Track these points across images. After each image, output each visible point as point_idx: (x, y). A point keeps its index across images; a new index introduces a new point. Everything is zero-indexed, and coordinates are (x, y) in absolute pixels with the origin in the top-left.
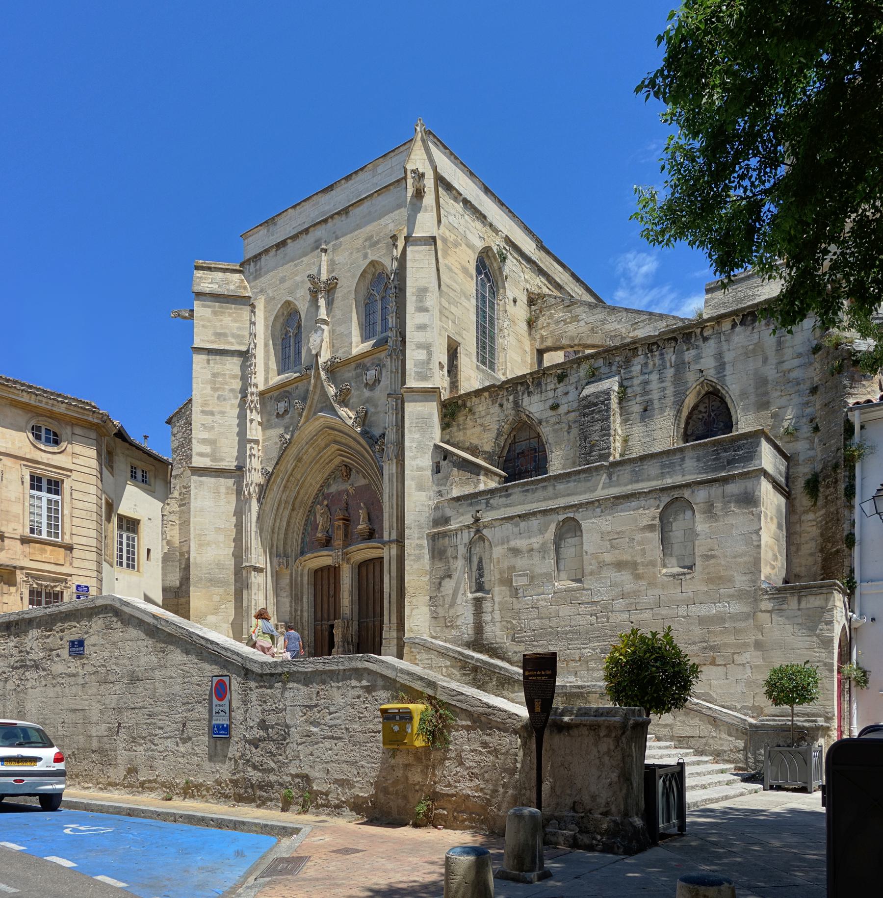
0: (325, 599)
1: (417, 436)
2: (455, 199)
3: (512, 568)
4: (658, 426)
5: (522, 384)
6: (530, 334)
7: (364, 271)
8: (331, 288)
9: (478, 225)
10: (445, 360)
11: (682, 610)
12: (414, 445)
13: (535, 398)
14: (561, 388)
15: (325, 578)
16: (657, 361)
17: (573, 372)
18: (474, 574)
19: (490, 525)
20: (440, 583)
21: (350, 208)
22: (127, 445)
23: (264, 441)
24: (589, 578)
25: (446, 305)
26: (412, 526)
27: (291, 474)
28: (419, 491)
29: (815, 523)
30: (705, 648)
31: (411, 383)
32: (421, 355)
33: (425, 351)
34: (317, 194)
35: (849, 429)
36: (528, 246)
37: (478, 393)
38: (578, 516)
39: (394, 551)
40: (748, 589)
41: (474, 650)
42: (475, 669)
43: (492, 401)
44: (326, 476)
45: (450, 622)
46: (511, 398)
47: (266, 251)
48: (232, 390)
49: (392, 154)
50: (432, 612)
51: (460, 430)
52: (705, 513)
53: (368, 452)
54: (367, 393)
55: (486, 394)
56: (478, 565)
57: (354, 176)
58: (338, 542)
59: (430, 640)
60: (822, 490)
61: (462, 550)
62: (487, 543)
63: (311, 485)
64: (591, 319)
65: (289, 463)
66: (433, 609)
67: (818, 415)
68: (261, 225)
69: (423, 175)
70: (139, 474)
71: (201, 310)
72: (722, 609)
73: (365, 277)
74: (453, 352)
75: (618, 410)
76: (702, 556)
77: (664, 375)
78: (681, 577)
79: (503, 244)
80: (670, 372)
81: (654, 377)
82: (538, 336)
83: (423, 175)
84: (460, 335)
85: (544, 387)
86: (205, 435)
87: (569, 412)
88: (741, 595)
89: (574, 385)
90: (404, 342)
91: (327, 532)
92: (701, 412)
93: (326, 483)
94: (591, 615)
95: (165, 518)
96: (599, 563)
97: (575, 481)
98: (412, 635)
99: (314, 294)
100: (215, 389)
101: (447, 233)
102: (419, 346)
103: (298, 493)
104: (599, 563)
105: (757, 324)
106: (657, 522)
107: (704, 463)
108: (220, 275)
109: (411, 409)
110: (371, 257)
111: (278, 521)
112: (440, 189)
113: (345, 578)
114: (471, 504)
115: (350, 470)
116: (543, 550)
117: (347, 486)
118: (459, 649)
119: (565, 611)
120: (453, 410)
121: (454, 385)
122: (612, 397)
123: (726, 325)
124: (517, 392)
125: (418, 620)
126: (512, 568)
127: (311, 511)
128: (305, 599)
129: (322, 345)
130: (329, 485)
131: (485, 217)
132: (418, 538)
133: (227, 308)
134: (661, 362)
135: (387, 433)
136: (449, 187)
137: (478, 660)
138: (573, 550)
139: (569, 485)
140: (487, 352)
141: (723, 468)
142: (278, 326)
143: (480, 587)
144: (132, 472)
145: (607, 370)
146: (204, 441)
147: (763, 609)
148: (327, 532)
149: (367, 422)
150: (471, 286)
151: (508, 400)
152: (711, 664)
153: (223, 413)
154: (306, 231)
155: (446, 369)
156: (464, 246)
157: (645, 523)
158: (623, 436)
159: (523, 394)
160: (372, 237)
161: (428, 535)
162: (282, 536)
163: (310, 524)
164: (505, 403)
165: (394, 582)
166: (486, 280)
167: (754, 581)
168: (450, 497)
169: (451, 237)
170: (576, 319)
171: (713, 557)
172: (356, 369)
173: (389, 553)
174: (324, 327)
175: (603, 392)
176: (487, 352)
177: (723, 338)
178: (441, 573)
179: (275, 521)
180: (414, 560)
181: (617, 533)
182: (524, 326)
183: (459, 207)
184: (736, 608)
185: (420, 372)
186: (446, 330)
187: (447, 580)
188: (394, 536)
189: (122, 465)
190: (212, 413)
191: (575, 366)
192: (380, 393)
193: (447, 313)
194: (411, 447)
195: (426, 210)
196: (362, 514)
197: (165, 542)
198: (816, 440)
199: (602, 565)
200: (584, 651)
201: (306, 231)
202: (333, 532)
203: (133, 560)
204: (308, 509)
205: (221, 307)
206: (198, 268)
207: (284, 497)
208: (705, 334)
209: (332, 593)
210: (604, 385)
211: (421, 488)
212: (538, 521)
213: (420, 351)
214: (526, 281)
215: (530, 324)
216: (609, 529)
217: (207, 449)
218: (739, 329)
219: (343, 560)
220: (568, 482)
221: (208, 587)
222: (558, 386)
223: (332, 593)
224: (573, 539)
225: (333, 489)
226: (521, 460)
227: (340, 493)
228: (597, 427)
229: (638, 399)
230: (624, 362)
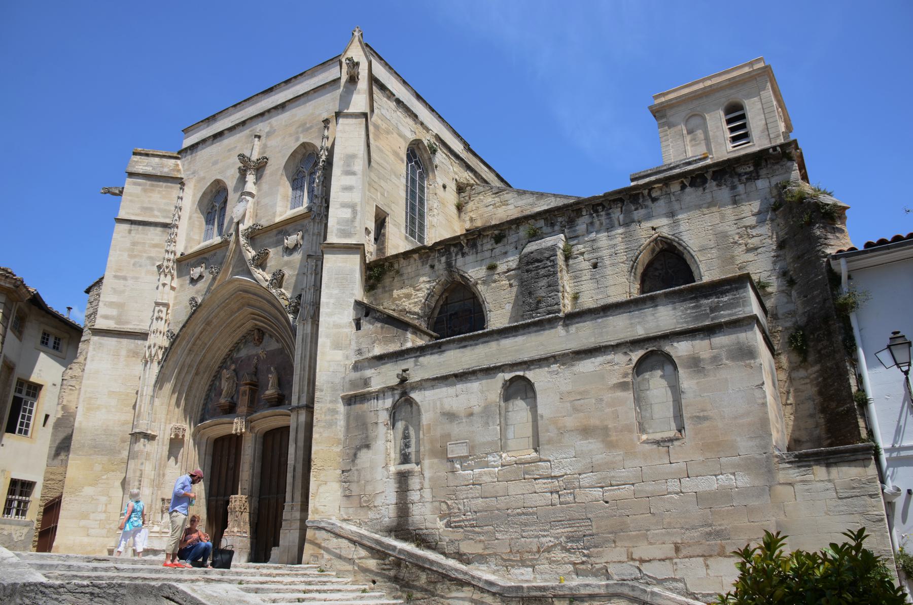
0: (224, 471)
1: (336, 292)
2: (389, 98)
3: (447, 437)
4: (611, 282)
5: (455, 245)
6: (459, 217)
7: (295, 152)
8: (260, 167)
9: (410, 121)
10: (372, 226)
11: (673, 485)
12: (332, 301)
14: (499, 248)
16: (603, 218)
17: (512, 232)
19: (421, 385)
20: (355, 455)
22: (43, 313)
23: (174, 304)
24: (546, 447)
25: (376, 179)
26: (325, 387)
27: (198, 338)
28: (335, 349)
29: (808, 381)
30: (709, 534)
31: (332, 239)
32: (347, 214)
33: (350, 210)
35: (835, 279)
36: (458, 147)
37: (406, 255)
38: (529, 375)
39: (303, 417)
40: (758, 457)
41: (397, 537)
42: (398, 563)
43: (423, 263)
44: (235, 341)
45: (365, 502)
46: (443, 259)
48: (322, 391)
50: (345, 489)
51: (385, 292)
52: (689, 367)
55: (416, 256)
56: (404, 433)
58: (242, 409)
59: (339, 524)
60: (812, 344)
63: (219, 349)
64: (520, 203)
65: (197, 327)
66: (346, 485)
67: (790, 268)
69: (358, 64)
70: (51, 342)
71: (131, 187)
72: (727, 483)
74: (381, 221)
75: (564, 267)
76: (692, 418)
78: (667, 444)
79: (433, 140)
82: (468, 218)
83: (358, 64)
84: (389, 207)
85: (479, 248)
86: (114, 298)
87: (509, 271)
88: (749, 466)
89: (514, 245)
90: (327, 202)
91: (232, 398)
92: (656, 269)
93: (236, 347)
94: (552, 493)
95: (65, 382)
96: (559, 429)
98: (317, 517)
99: (243, 173)
100: (131, 256)
101: (380, 122)
102: (344, 205)
103: (204, 356)
104: (559, 429)
105: (707, 185)
107: (682, 311)
108: (157, 160)
109: (331, 262)
112: (374, 87)
113: (246, 448)
115: (263, 334)
116: (486, 412)
117: (259, 351)
118: (377, 536)
119: (516, 488)
120: (378, 273)
121: (381, 249)
122: (558, 253)
123: (675, 187)
124: (450, 254)
125: (326, 499)
126: (447, 437)
127: (217, 376)
129: (244, 212)
130: (239, 350)
131: (416, 116)
132: (331, 402)
133: (157, 186)
134: (608, 221)
135: (303, 293)
136: (383, 87)
137: (401, 551)
140: (416, 219)
141: (706, 316)
142: (206, 201)
143: (405, 459)
144: (43, 338)
145: (549, 230)
146: (111, 304)
147: (782, 481)
148: (232, 398)
150: (402, 168)
151: (440, 261)
152: (719, 555)
153: (136, 279)
155: (372, 236)
156: (395, 135)
158: (575, 287)
159: (456, 255)
161: (343, 398)
163: (213, 389)
164: (437, 264)
165: (301, 453)
166: (416, 167)
167: (765, 447)
168: (371, 355)
169: (383, 126)
170: (505, 203)
171: (706, 418)
173: (295, 421)
174: (248, 198)
175: (547, 249)
176: (416, 219)
177: (673, 198)
178: (357, 443)
180: (324, 427)
181: (580, 393)
182: (454, 210)
183: (393, 105)
184: (743, 481)
185: (344, 230)
186: (374, 200)
188: (304, 401)
189: (33, 332)
190: (125, 278)
191: (514, 227)
193: (376, 186)
194: (328, 304)
195: (359, 93)
196: (272, 378)
197: (60, 406)
198: (794, 293)
199: (562, 432)
200: (543, 540)
202: (238, 398)
203: (28, 425)
205: (152, 185)
207: (188, 361)
208: (654, 195)
209: (231, 465)
210: (548, 242)
211: (337, 346)
213: (345, 210)
214: (456, 173)
215: (460, 208)
216: (570, 388)
217: (114, 312)
218: (689, 190)
220: (516, 336)
221: (90, 455)
222: (495, 246)
223: (231, 465)
225: (243, 353)
226: (456, 317)
227: (249, 358)
228: (543, 282)
229: (586, 256)
230: (568, 222)
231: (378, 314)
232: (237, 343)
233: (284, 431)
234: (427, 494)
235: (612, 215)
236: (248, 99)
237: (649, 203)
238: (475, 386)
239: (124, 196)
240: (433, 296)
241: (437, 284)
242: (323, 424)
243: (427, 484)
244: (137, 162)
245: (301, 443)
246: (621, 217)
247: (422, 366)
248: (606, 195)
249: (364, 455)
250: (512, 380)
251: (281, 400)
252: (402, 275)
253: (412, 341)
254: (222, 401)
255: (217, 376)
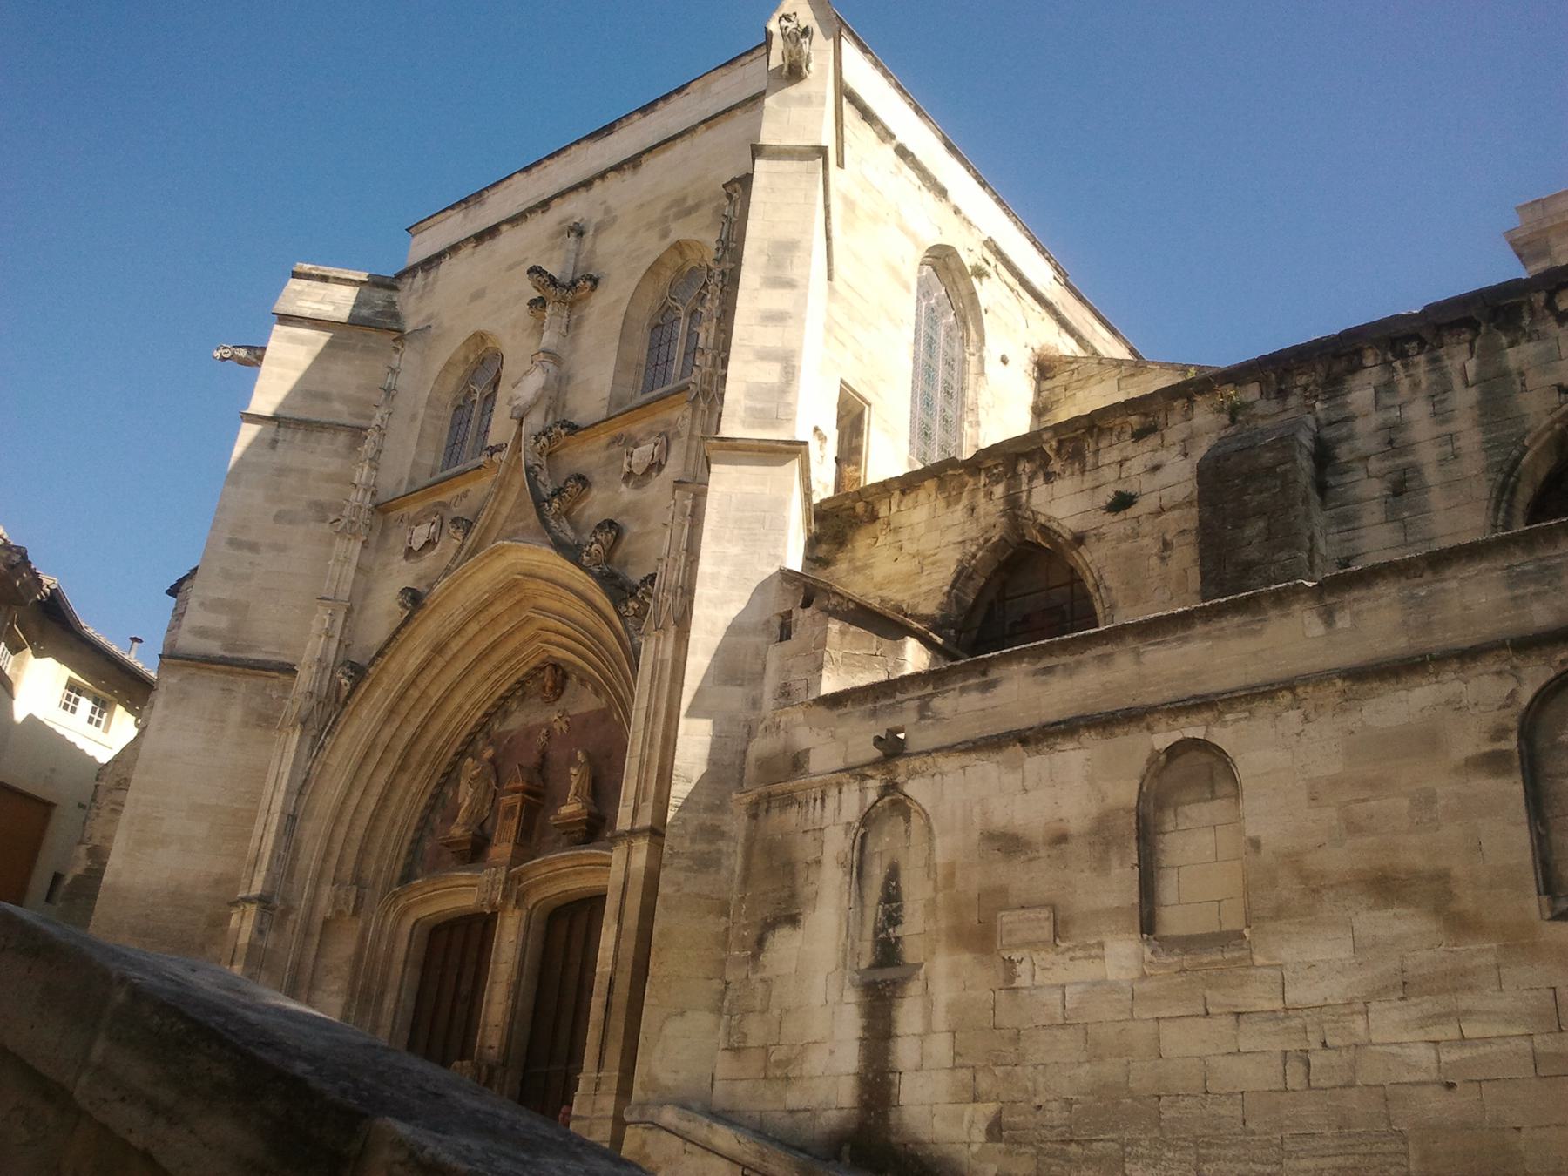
1: (734, 550)
5: (1028, 456)
12: (726, 570)
13: (1064, 486)
15: (461, 940)
18: (870, 914)
20: (760, 942)
21: (644, 158)
27: (413, 682)
28: (725, 682)
32: (770, 374)
34: (578, 142)
37: (907, 484)
38: (1222, 736)
39: (640, 859)
45: (779, 1064)
46: (999, 490)
47: (454, 249)
49: (748, 58)
53: (610, 623)
54: (627, 493)
55: (930, 484)
56: (886, 886)
57: (660, 105)
58: (501, 850)
61: (837, 843)
62: (916, 822)
68: (452, 207)
73: (658, 274)
77: (1448, 406)
80: (1464, 399)
81: (1418, 412)
85: (1090, 460)
87: (1161, 511)
89: (1178, 448)
93: (500, 708)
97: (1207, 636)
102: (765, 355)
103: (424, 727)
106: (1511, 744)
110: (674, 236)
111: (357, 794)
114: (874, 713)
115: (565, 676)
116: (1102, 833)
124: (1016, 476)
126: (995, 899)
128: (389, 1002)
130: (507, 715)
134: (1434, 377)
135: (662, 568)
136: (867, 115)
138: (1206, 838)
139: (1188, 647)
149: (618, 554)
154: (544, 205)
157: (1471, 751)
159: (1031, 479)
160: (684, 199)
162: (359, 832)
163: (438, 803)
165: (629, 945)
172: (609, 445)
179: (349, 794)
180: (688, 869)
185: (762, 411)
187: (784, 932)
188: (645, 820)
190: (253, 547)
191: (1178, 404)
192: (659, 486)
194: (714, 577)
201: (544, 205)
202: (493, 827)
204: (442, 768)
206: (295, 275)
207: (385, 736)
212: (1082, 754)
219: (505, 897)
220: (1185, 640)
224: (1206, 808)
225: (517, 721)
227: (529, 733)
229: (1374, 465)
231: (834, 601)
232: (504, 698)
233: (592, 904)
234: (941, 1046)
235: (1447, 362)
236: (557, 153)
237: (1551, 326)
238: (1073, 757)
239: (265, 365)
240: (970, 577)
241: (980, 548)
242: (685, 862)
243: (940, 1020)
244: (300, 292)
245: (631, 921)
246: (1472, 366)
247: (938, 719)
248: (1431, 309)
249: (785, 946)
250: (1173, 751)
251: (595, 828)
252: (897, 530)
253: (914, 657)
254: (457, 831)
255: (450, 776)
